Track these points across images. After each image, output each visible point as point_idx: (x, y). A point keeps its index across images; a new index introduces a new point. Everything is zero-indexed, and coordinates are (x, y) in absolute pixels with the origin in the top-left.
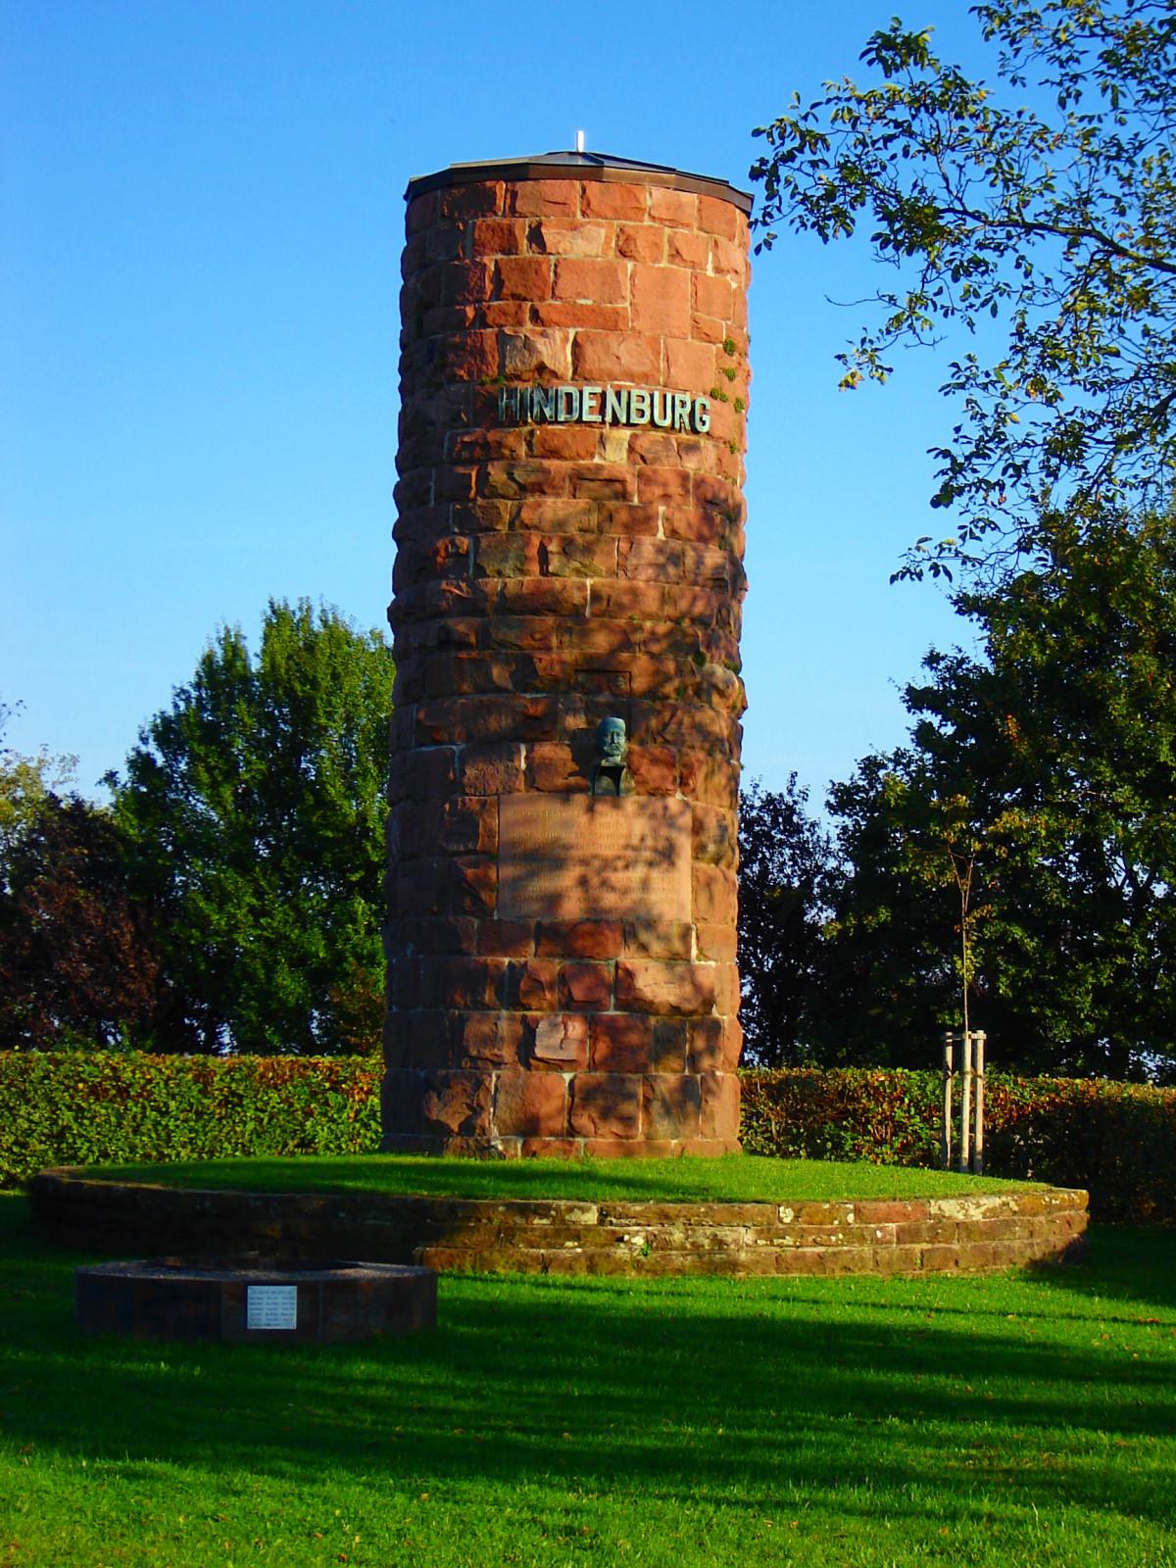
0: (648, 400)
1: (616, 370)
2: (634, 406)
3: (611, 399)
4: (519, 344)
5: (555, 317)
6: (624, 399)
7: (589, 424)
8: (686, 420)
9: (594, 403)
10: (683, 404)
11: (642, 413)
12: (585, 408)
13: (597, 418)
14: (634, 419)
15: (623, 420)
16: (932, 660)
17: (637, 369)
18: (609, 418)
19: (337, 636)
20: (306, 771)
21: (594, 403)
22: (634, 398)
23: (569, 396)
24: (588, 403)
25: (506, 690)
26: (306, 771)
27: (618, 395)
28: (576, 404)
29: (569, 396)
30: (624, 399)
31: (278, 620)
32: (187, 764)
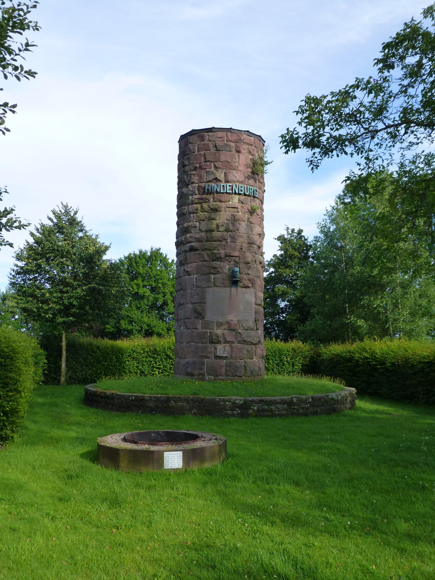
0: (243, 188)
1: (235, 180)
2: (240, 189)
3: (234, 187)
4: (210, 173)
5: (220, 166)
6: (237, 187)
7: (229, 193)
8: (252, 193)
9: (230, 188)
10: (251, 189)
11: (242, 190)
12: (228, 189)
13: (231, 192)
14: (240, 192)
15: (237, 192)
16: (274, 256)
17: (240, 180)
18: (234, 192)
19: (156, 256)
20: (49, 317)
21: (230, 188)
22: (240, 187)
23: (223, 186)
24: (228, 188)
25: (208, 261)
26: (49, 317)
27: (236, 186)
28: (225, 188)
29: (223, 186)
30: (237, 187)
31: (140, 252)
32: (286, 306)
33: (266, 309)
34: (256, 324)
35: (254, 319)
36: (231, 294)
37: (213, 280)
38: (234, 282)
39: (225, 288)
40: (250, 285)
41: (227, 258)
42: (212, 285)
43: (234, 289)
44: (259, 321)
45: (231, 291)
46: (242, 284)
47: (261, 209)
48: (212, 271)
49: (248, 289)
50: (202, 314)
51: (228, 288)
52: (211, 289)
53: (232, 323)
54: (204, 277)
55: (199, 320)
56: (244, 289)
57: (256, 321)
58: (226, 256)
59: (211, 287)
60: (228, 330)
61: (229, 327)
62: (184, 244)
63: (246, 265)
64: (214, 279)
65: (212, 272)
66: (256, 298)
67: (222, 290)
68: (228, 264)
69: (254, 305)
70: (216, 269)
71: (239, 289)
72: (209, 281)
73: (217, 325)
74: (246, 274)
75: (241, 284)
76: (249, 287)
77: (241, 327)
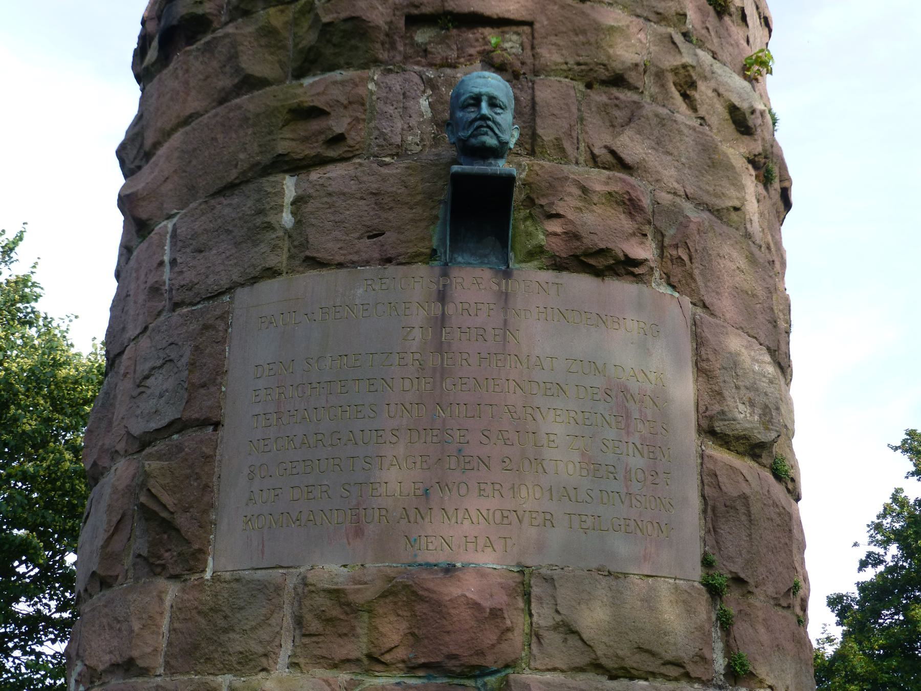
33: (823, 682)
34: (725, 623)
35: (697, 573)
36: (442, 321)
37: (287, 219)
38: (478, 210)
39: (391, 269)
40: (644, 251)
41: (422, 36)
42: (280, 259)
43: (473, 282)
44: (759, 601)
45: (442, 297)
46: (555, 226)
47: (765, 178)
48: (286, 143)
49: (621, 289)
50: (181, 520)
51: (421, 270)
52: (269, 289)
53: (451, 590)
54: (227, 207)
55: (161, 582)
56: (580, 284)
57: (714, 591)
58: (415, 21)
59: (272, 273)
60: (412, 669)
61: (414, 637)
62: (202, 115)
63: (599, 96)
64: (298, 202)
65: (283, 147)
66: (702, 370)
67: (360, 288)
68: (430, 84)
69: (687, 438)
70: (315, 125)
71: (532, 278)
72: (259, 228)
73: (299, 622)
74: (594, 160)
75: (547, 234)
76: (626, 267)
77: (553, 639)
